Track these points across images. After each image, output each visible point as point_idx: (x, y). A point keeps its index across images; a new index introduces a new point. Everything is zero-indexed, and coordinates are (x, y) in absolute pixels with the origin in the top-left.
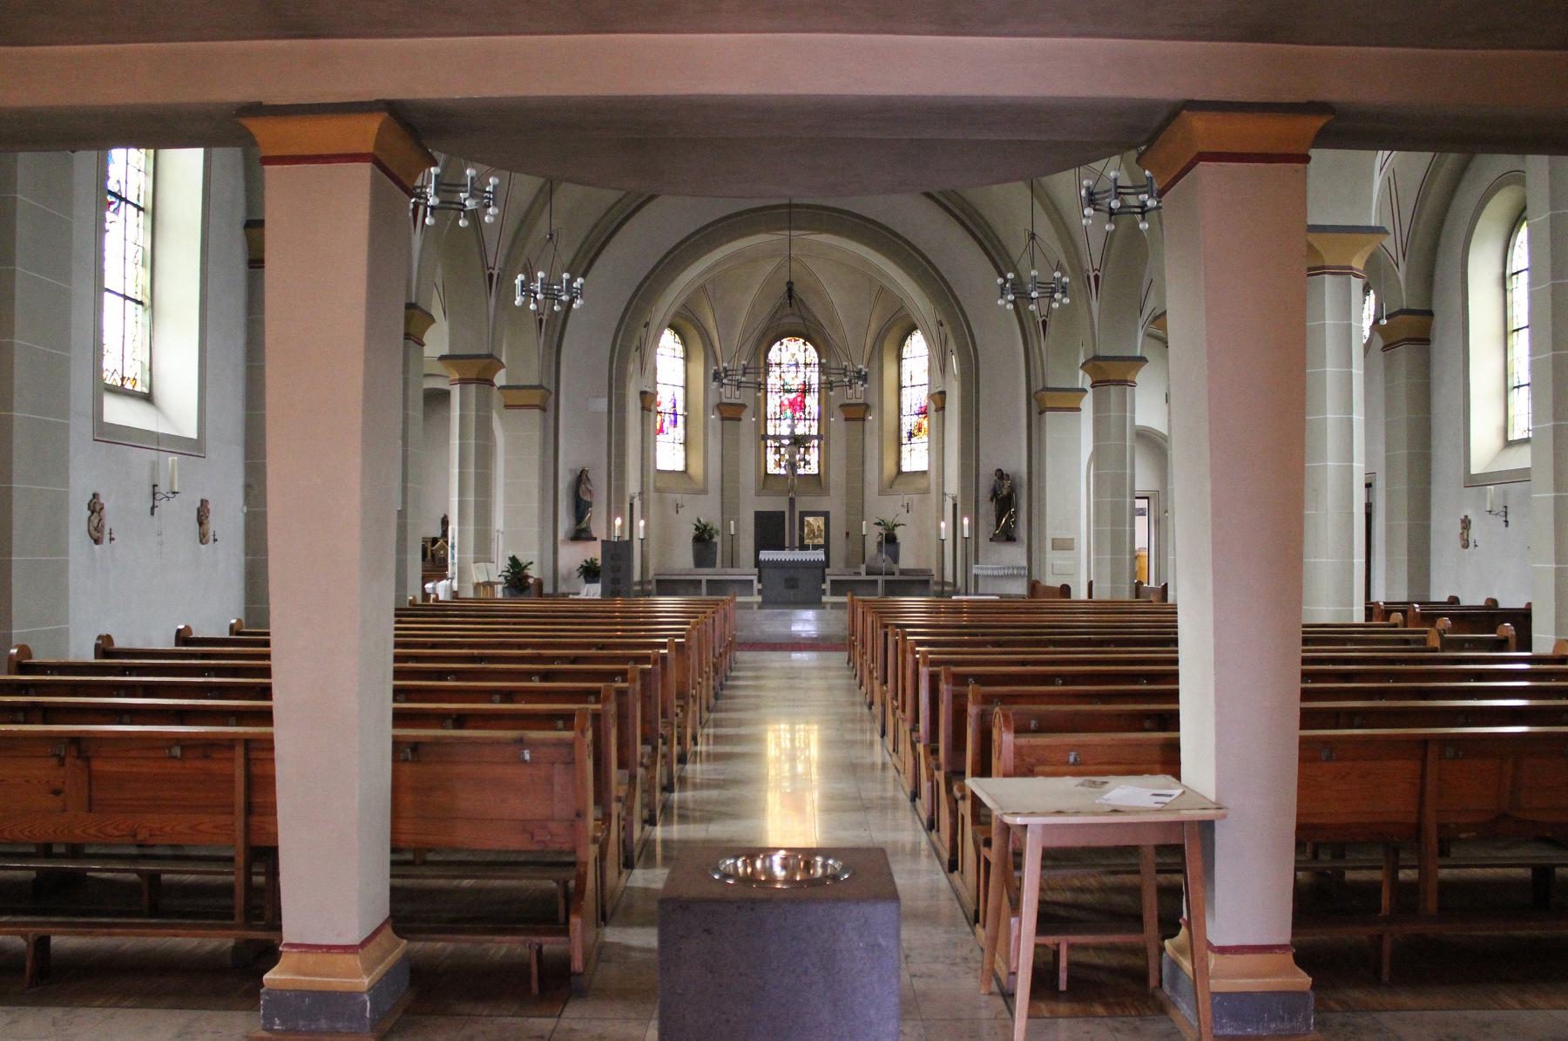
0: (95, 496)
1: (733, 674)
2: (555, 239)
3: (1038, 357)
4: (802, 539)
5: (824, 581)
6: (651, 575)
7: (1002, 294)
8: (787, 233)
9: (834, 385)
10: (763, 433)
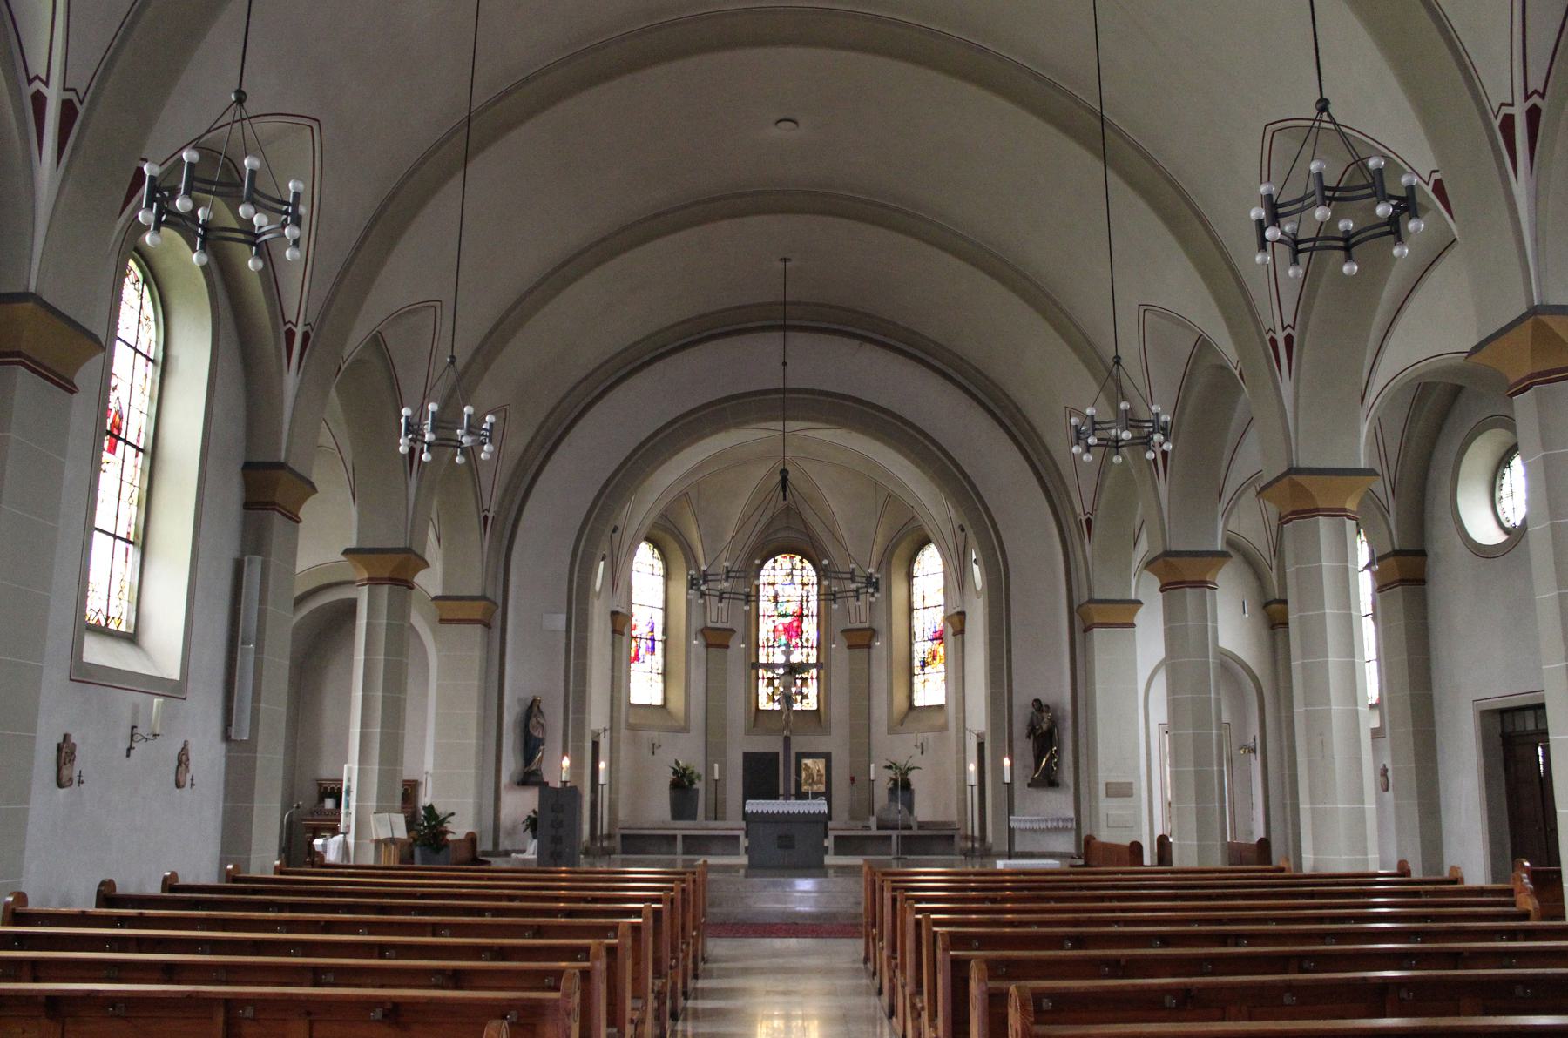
0: (66, 737)
3: (1082, 564)
4: (799, 785)
6: (618, 833)
7: (1078, 438)
8: (778, 425)
9: (838, 595)
10: (753, 660)
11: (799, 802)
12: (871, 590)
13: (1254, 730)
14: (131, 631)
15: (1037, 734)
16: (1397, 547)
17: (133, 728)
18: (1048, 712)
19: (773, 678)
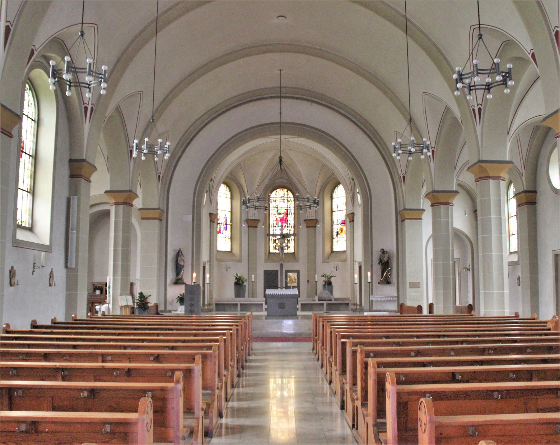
0: (12, 268)
1: (251, 358)
2: (155, 121)
4: (286, 283)
5: (298, 304)
6: (214, 302)
8: (278, 137)
9: (302, 207)
10: (268, 233)
11: (287, 290)
12: (316, 205)
13: (469, 261)
14: (30, 226)
15: (383, 263)
16: (525, 190)
17: (34, 264)
18: (387, 254)
19: (276, 240)
